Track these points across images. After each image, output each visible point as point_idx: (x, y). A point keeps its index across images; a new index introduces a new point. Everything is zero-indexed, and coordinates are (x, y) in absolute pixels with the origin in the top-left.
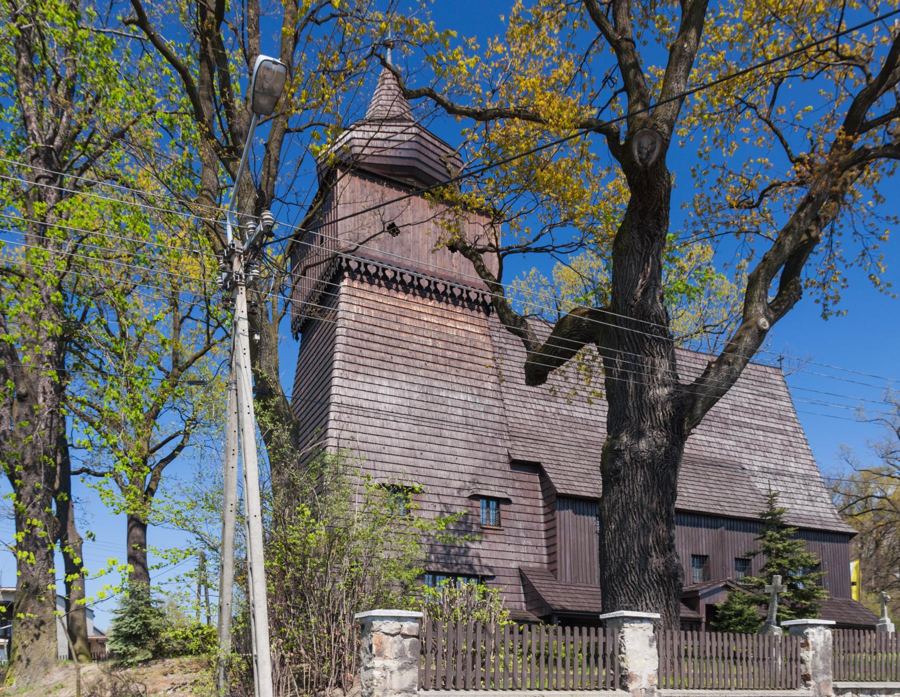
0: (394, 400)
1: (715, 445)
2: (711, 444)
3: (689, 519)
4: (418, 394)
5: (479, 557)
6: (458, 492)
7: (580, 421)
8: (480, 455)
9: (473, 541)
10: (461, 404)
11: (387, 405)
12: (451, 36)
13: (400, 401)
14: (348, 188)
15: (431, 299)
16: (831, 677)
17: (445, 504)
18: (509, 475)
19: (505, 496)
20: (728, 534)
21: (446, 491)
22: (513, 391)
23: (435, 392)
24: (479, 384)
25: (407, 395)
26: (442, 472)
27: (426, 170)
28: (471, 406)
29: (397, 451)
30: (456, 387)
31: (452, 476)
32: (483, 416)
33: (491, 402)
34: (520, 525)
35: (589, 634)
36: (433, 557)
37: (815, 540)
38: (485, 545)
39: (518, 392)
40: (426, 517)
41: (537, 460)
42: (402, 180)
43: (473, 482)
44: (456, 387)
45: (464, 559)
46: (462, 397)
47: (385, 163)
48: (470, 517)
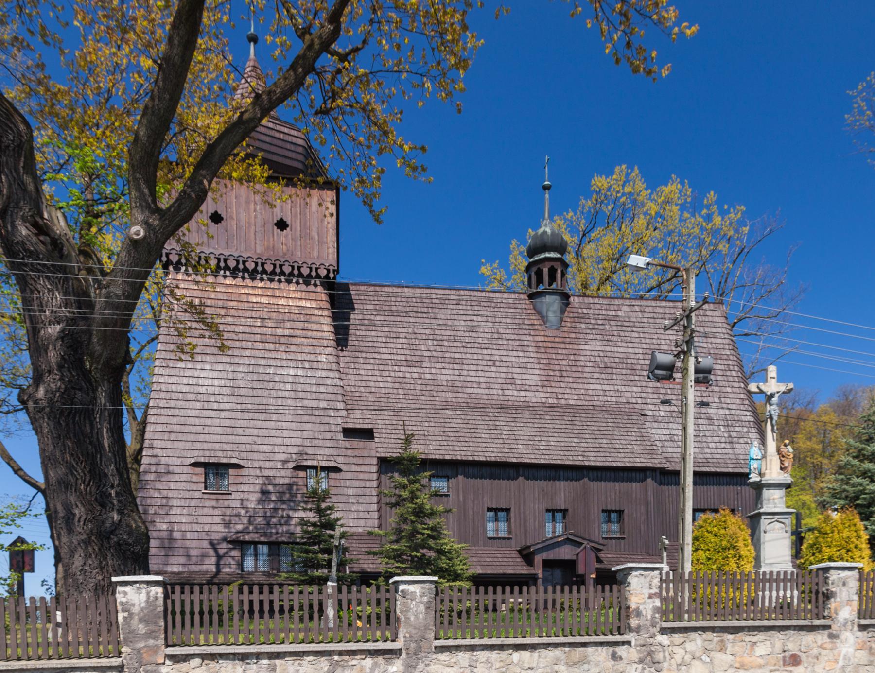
0: (216, 382)
1: (612, 393)
2: (607, 393)
3: (486, 471)
4: (243, 374)
7: (445, 383)
8: (309, 426)
9: (295, 510)
10: (290, 379)
11: (209, 388)
12: (78, 21)
13: (223, 382)
15: (262, 280)
16: (161, 642)
17: (268, 477)
18: (342, 444)
19: (333, 464)
20: (595, 486)
21: (268, 465)
22: (372, 361)
23: (261, 370)
24: (312, 357)
25: (230, 376)
26: (265, 447)
28: (302, 380)
29: (219, 430)
30: (284, 363)
31: (276, 449)
32: (314, 389)
33: (324, 374)
34: (351, 491)
35: (571, 592)
36: (251, 528)
37: (535, 478)
39: (377, 362)
40: (245, 490)
41: (370, 426)
44: (284, 363)
45: (285, 528)
46: (292, 372)
48: (295, 487)
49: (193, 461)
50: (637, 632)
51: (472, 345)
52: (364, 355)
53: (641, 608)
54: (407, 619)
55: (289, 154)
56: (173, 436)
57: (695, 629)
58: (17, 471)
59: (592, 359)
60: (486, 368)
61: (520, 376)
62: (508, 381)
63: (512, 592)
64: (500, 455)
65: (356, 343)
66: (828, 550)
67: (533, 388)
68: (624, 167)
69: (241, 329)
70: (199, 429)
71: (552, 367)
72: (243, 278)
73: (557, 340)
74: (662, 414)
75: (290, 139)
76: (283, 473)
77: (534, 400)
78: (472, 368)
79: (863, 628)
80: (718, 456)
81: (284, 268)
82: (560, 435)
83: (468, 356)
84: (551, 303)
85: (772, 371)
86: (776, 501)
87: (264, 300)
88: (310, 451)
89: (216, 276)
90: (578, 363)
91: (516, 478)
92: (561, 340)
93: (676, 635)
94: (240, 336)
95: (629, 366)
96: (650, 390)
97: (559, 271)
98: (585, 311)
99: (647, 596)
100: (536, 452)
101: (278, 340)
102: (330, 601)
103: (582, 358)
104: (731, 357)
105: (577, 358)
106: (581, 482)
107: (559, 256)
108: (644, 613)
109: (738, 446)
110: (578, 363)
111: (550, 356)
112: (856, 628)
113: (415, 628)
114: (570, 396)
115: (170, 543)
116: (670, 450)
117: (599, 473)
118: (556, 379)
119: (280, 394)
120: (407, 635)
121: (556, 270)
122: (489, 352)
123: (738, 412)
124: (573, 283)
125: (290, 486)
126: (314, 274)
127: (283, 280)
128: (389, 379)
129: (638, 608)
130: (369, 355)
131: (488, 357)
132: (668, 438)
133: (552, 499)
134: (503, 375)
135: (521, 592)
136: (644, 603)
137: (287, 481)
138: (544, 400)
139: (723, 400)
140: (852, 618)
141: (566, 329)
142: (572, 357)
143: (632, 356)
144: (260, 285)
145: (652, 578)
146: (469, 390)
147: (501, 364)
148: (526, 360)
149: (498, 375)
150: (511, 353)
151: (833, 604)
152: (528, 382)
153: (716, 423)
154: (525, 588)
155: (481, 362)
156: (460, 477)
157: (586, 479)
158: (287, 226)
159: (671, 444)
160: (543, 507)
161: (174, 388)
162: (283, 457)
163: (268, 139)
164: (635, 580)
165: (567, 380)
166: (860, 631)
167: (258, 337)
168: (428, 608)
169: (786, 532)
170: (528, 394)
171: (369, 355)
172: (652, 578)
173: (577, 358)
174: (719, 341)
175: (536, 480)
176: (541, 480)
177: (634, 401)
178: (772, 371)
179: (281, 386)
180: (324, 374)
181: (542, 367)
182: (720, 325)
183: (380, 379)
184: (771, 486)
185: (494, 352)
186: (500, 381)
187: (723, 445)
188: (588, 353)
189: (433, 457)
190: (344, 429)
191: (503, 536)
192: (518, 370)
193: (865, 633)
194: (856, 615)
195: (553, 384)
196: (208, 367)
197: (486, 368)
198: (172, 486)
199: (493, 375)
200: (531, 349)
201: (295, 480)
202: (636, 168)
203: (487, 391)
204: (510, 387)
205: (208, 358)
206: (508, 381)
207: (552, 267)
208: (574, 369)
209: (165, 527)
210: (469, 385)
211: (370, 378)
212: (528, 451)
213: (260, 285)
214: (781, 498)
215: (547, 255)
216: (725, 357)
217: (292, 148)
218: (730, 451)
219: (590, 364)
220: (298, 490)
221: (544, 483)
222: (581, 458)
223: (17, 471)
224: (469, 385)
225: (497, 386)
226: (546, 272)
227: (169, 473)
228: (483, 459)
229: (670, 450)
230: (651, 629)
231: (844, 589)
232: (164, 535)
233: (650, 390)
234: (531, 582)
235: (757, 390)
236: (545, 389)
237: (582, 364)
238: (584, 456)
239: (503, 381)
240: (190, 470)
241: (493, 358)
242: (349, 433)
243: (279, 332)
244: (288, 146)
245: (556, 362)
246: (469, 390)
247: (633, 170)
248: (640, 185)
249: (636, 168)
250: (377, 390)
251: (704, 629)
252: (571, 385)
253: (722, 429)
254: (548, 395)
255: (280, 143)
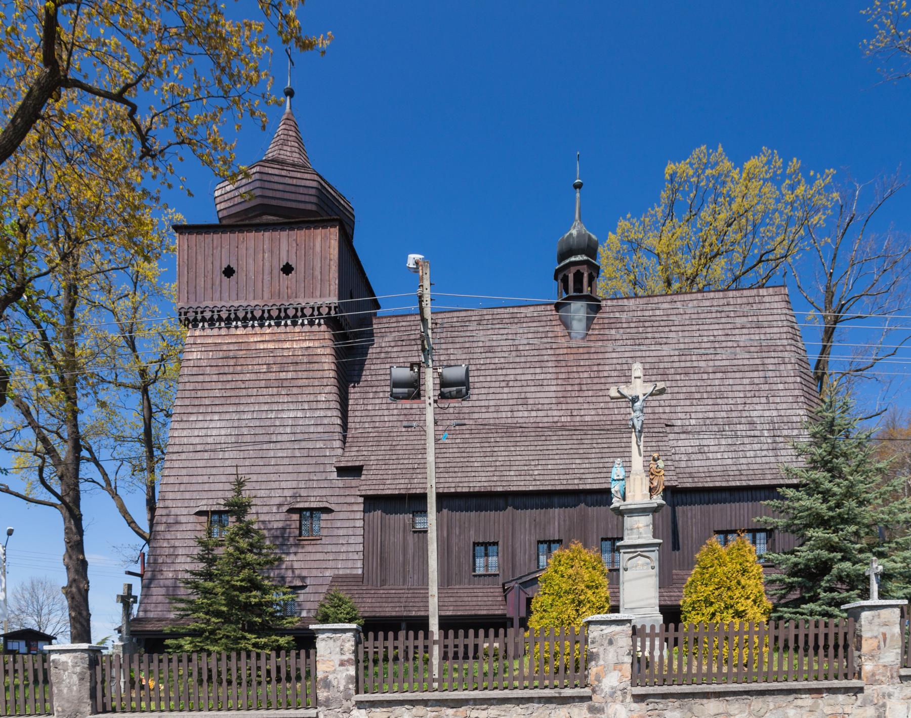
0: (223, 432)
3: (474, 502)
5: (293, 570)
6: (278, 509)
13: (229, 431)
14: (326, 241)
15: (270, 326)
17: (263, 522)
18: (340, 484)
27: (274, 202)
28: (301, 422)
30: (285, 407)
33: (322, 413)
37: (526, 507)
38: (300, 557)
42: (257, 221)
43: (294, 497)
45: (277, 572)
46: (292, 414)
47: (243, 208)
48: (288, 530)
49: (198, 510)
50: (327, 706)
51: (487, 367)
52: (374, 389)
53: (331, 677)
54: (60, 691)
55: (300, 198)
56: (182, 488)
57: (401, 703)
58: (131, 523)
59: (618, 367)
60: (499, 390)
61: (534, 395)
62: (520, 402)
63: (486, 636)
64: (486, 484)
65: (369, 378)
66: (703, 588)
67: (546, 407)
68: (703, 148)
69: (248, 377)
70: (205, 479)
71: (571, 382)
72: (203, 328)
73: (581, 350)
74: (693, 422)
75: (303, 183)
76: (278, 517)
77: (546, 419)
78: (483, 391)
79: (639, 698)
80: (756, 467)
81: (272, 313)
82: (562, 456)
83: (482, 379)
84: (578, 309)
85: (637, 370)
86: (641, 530)
87: (271, 346)
88: (303, 493)
89: (229, 328)
90: (601, 374)
91: (505, 509)
92: (585, 350)
93: (378, 710)
94: (247, 385)
95: (661, 371)
96: (682, 396)
97: (586, 275)
98: (617, 315)
99: (337, 663)
100: (528, 478)
101: (281, 384)
102: (436, 637)
103: (607, 368)
104: (788, 348)
105: (601, 368)
106: (578, 508)
107: (585, 258)
108: (335, 683)
109: (783, 452)
110: (601, 374)
111: (570, 369)
112: (629, 699)
113: (68, 701)
114: (586, 412)
115: (174, 590)
116: (696, 463)
117: (599, 497)
118: (573, 394)
119: (279, 438)
120: (60, 709)
121: (583, 274)
122: (504, 372)
123: (789, 412)
124: (601, 288)
125: (284, 529)
126: (199, 317)
127: (256, 325)
128: (395, 412)
129: (327, 677)
130: (379, 389)
131: (502, 378)
132: (696, 449)
133: (544, 529)
134: (515, 396)
135: (496, 635)
136: (334, 672)
137: (280, 525)
138: (556, 419)
139: (771, 399)
140: (622, 686)
141: (593, 338)
142: (595, 368)
143: (666, 359)
144: (268, 331)
145: (343, 641)
146: (476, 416)
147: (515, 384)
148: (543, 377)
149: (510, 396)
150: (527, 371)
151: (594, 669)
152: (541, 401)
153: (759, 427)
154: (501, 631)
155: (493, 384)
156: (510, 508)
157: (583, 505)
158: (293, 269)
159: (700, 456)
160: (534, 539)
161: (185, 440)
162: (277, 501)
163: (281, 187)
164: (323, 645)
165: (586, 394)
166: (635, 702)
167: (263, 384)
168: (82, 679)
169: (653, 568)
170: (540, 413)
171: (379, 389)
172: (343, 641)
173: (601, 368)
174: (775, 330)
175: (527, 509)
176: (532, 509)
177: (661, 410)
178: (637, 370)
179: (281, 430)
180: (322, 413)
181: (560, 382)
182: (779, 311)
183: (386, 412)
184: (632, 512)
185: (509, 372)
186: (511, 402)
187: (764, 453)
188: (615, 361)
189: (414, 491)
190: (337, 468)
191: (493, 572)
192: (533, 389)
193: (643, 705)
194: (629, 683)
195: (569, 400)
196: (216, 417)
197: (499, 390)
198: (179, 535)
199: (505, 396)
200: (550, 364)
201: (288, 522)
202: (720, 146)
203: (495, 415)
204: (520, 408)
205: (217, 409)
206: (520, 402)
207: (578, 271)
208: (595, 381)
209: (170, 575)
210: (476, 410)
211: (376, 413)
212: (519, 478)
213: (268, 331)
214: (648, 526)
215: (573, 259)
216: (781, 348)
217: (305, 191)
218: (773, 460)
219: (616, 374)
220: (290, 533)
221: (536, 513)
222: (576, 481)
223: (131, 523)
224: (476, 410)
225: (507, 408)
226: (576, 277)
227: (177, 523)
228: (467, 490)
229: (696, 463)
230: (344, 702)
231: (611, 649)
232: (169, 583)
233: (682, 396)
234: (509, 623)
235: (618, 395)
236: (560, 407)
237: (606, 374)
238: (580, 479)
239: (514, 402)
240: (193, 519)
241: (508, 378)
242: (343, 471)
243: (283, 375)
244: (301, 190)
245: (576, 375)
246: (476, 416)
247: (716, 149)
248: (727, 164)
249: (720, 146)
250: (381, 424)
251: (413, 703)
252: (589, 400)
253: (766, 433)
254: (561, 413)
255: (293, 189)
